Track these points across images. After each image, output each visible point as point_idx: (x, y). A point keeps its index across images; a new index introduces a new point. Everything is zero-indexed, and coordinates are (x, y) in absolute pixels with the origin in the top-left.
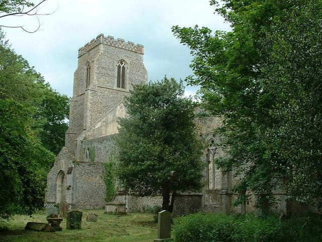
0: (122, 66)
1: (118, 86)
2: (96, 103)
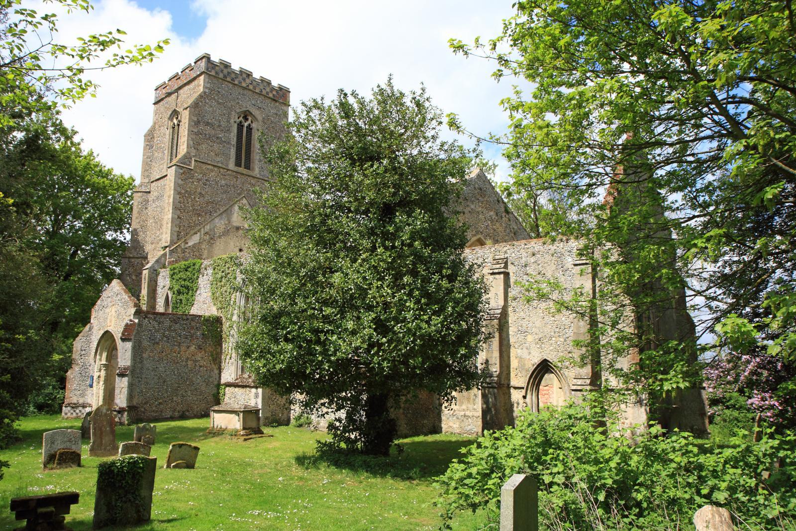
0: (246, 124)
1: (238, 164)
2: (190, 194)
